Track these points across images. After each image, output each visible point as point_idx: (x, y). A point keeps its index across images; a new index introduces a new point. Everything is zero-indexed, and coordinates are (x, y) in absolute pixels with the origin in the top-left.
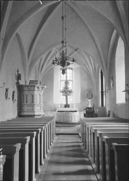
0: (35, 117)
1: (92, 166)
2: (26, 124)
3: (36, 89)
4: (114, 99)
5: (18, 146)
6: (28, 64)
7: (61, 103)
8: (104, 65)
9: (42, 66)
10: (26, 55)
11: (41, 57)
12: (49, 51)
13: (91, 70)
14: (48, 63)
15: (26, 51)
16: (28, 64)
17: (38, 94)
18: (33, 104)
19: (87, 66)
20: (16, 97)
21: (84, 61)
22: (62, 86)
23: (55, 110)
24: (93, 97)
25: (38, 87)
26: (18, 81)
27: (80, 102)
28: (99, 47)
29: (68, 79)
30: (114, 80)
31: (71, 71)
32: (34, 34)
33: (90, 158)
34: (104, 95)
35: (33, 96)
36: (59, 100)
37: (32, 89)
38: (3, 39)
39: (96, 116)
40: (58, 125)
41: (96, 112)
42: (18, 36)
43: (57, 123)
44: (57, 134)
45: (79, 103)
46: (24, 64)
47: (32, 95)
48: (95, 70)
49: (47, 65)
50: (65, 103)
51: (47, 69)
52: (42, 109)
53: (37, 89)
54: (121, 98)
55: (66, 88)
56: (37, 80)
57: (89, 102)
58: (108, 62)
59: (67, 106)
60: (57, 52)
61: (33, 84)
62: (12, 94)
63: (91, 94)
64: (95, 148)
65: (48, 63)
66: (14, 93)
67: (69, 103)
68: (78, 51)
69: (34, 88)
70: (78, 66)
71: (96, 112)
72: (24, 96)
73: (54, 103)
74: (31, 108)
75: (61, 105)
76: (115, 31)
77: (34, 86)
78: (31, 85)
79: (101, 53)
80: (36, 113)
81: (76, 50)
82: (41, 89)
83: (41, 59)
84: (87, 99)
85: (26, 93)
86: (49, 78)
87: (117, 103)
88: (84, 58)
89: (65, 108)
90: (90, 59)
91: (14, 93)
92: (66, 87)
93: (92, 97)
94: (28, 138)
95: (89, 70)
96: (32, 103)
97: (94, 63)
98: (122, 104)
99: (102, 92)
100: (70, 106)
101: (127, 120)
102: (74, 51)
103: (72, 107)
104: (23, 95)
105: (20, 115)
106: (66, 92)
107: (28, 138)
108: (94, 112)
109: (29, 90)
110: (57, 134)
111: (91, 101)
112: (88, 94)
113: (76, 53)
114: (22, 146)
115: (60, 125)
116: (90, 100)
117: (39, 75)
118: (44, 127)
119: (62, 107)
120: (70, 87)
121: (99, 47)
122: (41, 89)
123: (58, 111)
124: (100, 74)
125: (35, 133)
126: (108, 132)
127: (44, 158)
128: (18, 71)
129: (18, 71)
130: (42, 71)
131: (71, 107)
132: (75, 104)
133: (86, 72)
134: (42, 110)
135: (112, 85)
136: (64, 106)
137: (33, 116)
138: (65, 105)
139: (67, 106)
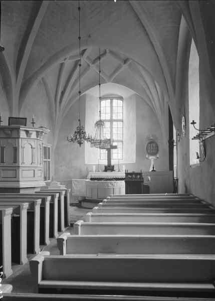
0: (22, 192)
3: (23, 134)
4: (186, 157)
9: (63, 93)
10: (10, 69)
13: (156, 99)
14: (72, 88)
18: (14, 165)
21: (142, 83)
23: (86, 177)
24: (160, 152)
25: (27, 132)
27: (135, 161)
28: (157, 44)
30: (186, 116)
31: (120, 102)
35: (16, 150)
37: (14, 135)
38: (79, 66)
39: (147, 190)
41: (145, 183)
47: (14, 148)
49: (71, 92)
50: (105, 163)
51: (70, 100)
52: (38, 173)
53: (25, 135)
55: (78, 132)
56: (26, 117)
57: (150, 160)
59: (109, 168)
60: (89, 65)
63: (154, 145)
65: (72, 88)
67: (113, 163)
68: (128, 63)
69: (18, 133)
70: (132, 92)
71: (145, 183)
73: (86, 162)
74: (10, 174)
75: (98, 166)
77: (18, 129)
78: (13, 126)
80: (22, 184)
81: (125, 61)
82: (34, 135)
84: (147, 156)
88: (142, 76)
89: (106, 173)
93: (158, 150)
95: (151, 98)
96: (14, 163)
100: (115, 169)
101: (207, 206)
102: (122, 64)
103: (119, 171)
108: (143, 182)
109: (8, 136)
111: (155, 160)
112: (149, 147)
113: (125, 67)
116: (152, 158)
117: (56, 110)
119: (99, 171)
121: (157, 44)
122: (34, 135)
123: (92, 179)
130: (63, 103)
131: (118, 170)
132: (124, 164)
135: (184, 126)
136: (104, 168)
138: (106, 167)
139: (109, 168)
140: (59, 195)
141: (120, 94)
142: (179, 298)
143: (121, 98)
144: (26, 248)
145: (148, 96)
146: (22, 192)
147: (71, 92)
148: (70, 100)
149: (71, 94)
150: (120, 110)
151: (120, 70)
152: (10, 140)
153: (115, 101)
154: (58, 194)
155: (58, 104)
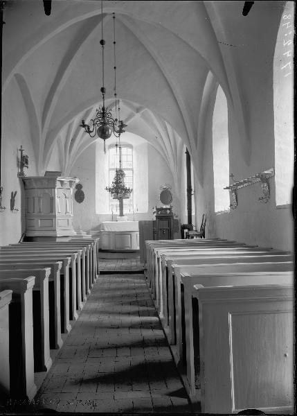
0: (58, 240)
1: (164, 332)
2: (36, 252)
3: (58, 185)
5: (31, 281)
6: (42, 138)
7: (118, 167)
8: (192, 141)
9: (73, 140)
11: (69, 122)
12: (86, 110)
13: (169, 150)
15: (38, 111)
16: (42, 138)
17: (63, 198)
18: (51, 214)
19: (160, 142)
20: (18, 204)
22: (109, 181)
25: (62, 182)
26: (22, 170)
29: (124, 166)
31: (130, 150)
32: (54, 74)
33: (161, 316)
34: (193, 196)
36: (104, 205)
40: (104, 255)
42: (20, 80)
43: (101, 251)
44: (102, 273)
45: (145, 214)
46: (34, 140)
48: (176, 149)
49: (81, 140)
51: (80, 148)
54: (223, 202)
58: (199, 132)
61: (51, 178)
62: (9, 198)
64: (177, 317)
66: (13, 196)
72: (34, 198)
73: (97, 212)
74: (47, 223)
76: (210, 75)
79: (187, 119)
82: (67, 186)
83: (70, 126)
85: (37, 193)
86: (87, 165)
87: (216, 211)
88: (153, 125)
90: (166, 130)
91: (13, 196)
92: (117, 180)
94: (48, 271)
97: (174, 135)
98: (224, 214)
99: (189, 190)
102: (135, 113)
104: (35, 194)
105: (27, 239)
106: (119, 191)
107: (48, 271)
110: (102, 273)
114: (36, 280)
115: (109, 255)
118: (76, 254)
120: (127, 182)
124: (185, 156)
125: (60, 263)
126: (229, 351)
127: (77, 309)
128: (22, 151)
129: (22, 151)
133: (159, 152)
134: (71, 227)
137: (56, 237)
140: (63, 265)
141: (130, 143)
142: (135, 387)
143: (131, 146)
144: (32, 324)
145: (165, 155)
146: (58, 240)
147: (81, 140)
148: (80, 148)
149: (82, 141)
150: (130, 158)
151: (133, 119)
152: (47, 191)
153: (124, 150)
154: (60, 263)
155: (68, 154)
